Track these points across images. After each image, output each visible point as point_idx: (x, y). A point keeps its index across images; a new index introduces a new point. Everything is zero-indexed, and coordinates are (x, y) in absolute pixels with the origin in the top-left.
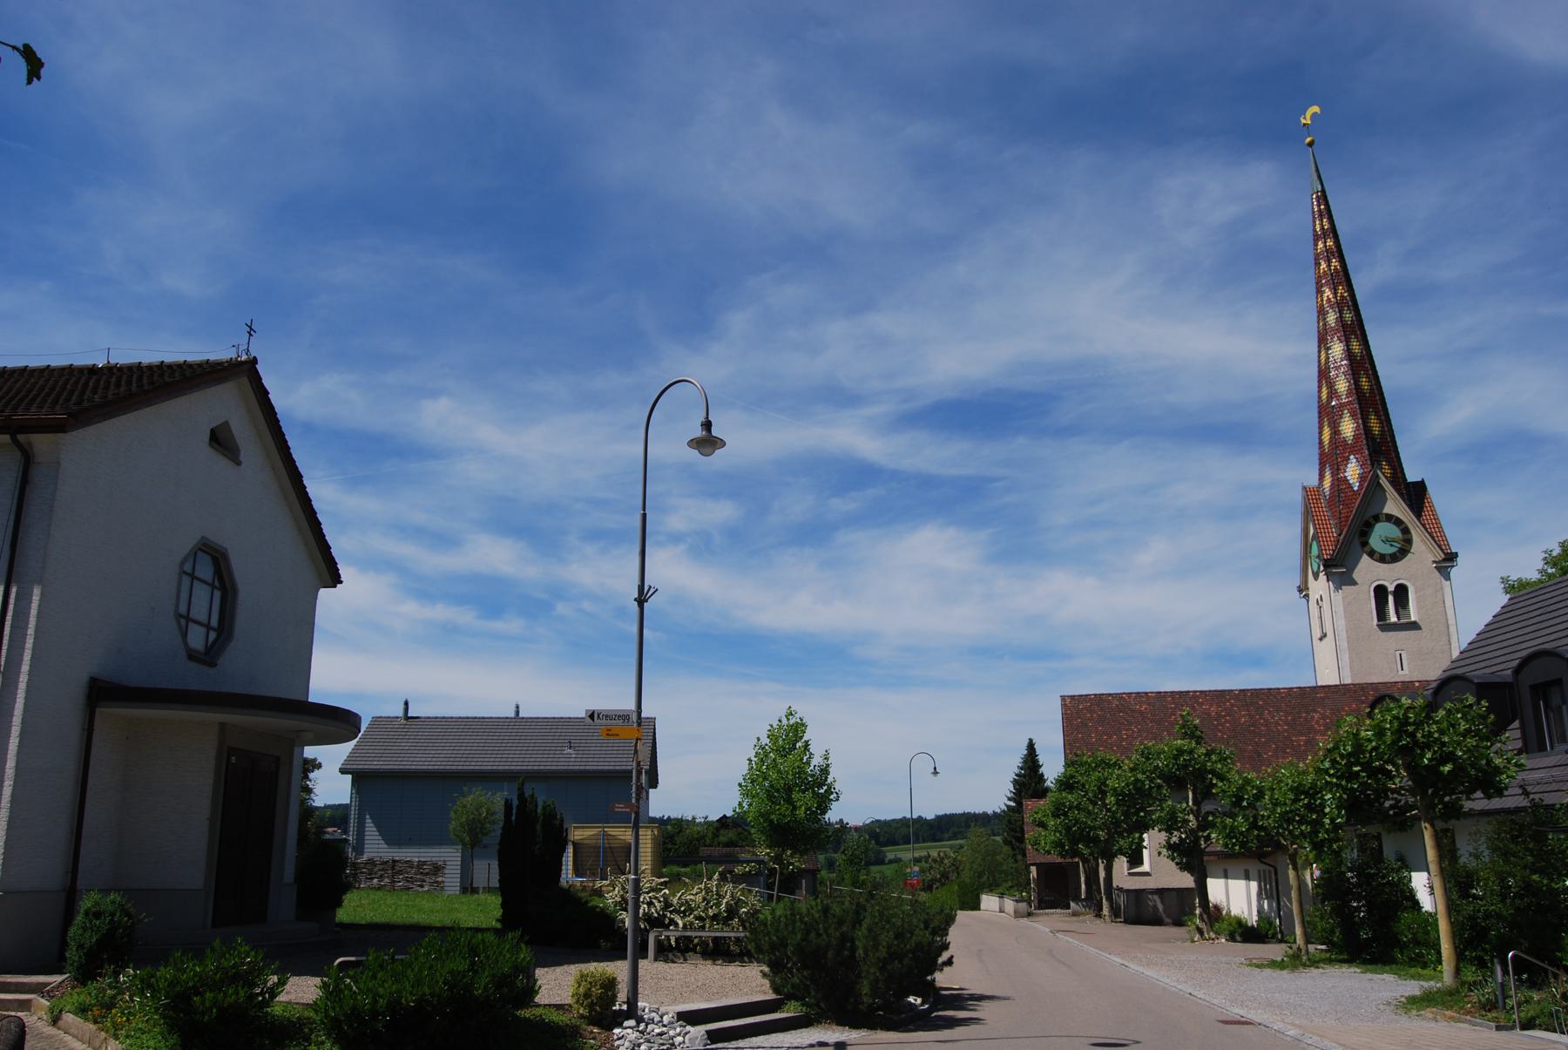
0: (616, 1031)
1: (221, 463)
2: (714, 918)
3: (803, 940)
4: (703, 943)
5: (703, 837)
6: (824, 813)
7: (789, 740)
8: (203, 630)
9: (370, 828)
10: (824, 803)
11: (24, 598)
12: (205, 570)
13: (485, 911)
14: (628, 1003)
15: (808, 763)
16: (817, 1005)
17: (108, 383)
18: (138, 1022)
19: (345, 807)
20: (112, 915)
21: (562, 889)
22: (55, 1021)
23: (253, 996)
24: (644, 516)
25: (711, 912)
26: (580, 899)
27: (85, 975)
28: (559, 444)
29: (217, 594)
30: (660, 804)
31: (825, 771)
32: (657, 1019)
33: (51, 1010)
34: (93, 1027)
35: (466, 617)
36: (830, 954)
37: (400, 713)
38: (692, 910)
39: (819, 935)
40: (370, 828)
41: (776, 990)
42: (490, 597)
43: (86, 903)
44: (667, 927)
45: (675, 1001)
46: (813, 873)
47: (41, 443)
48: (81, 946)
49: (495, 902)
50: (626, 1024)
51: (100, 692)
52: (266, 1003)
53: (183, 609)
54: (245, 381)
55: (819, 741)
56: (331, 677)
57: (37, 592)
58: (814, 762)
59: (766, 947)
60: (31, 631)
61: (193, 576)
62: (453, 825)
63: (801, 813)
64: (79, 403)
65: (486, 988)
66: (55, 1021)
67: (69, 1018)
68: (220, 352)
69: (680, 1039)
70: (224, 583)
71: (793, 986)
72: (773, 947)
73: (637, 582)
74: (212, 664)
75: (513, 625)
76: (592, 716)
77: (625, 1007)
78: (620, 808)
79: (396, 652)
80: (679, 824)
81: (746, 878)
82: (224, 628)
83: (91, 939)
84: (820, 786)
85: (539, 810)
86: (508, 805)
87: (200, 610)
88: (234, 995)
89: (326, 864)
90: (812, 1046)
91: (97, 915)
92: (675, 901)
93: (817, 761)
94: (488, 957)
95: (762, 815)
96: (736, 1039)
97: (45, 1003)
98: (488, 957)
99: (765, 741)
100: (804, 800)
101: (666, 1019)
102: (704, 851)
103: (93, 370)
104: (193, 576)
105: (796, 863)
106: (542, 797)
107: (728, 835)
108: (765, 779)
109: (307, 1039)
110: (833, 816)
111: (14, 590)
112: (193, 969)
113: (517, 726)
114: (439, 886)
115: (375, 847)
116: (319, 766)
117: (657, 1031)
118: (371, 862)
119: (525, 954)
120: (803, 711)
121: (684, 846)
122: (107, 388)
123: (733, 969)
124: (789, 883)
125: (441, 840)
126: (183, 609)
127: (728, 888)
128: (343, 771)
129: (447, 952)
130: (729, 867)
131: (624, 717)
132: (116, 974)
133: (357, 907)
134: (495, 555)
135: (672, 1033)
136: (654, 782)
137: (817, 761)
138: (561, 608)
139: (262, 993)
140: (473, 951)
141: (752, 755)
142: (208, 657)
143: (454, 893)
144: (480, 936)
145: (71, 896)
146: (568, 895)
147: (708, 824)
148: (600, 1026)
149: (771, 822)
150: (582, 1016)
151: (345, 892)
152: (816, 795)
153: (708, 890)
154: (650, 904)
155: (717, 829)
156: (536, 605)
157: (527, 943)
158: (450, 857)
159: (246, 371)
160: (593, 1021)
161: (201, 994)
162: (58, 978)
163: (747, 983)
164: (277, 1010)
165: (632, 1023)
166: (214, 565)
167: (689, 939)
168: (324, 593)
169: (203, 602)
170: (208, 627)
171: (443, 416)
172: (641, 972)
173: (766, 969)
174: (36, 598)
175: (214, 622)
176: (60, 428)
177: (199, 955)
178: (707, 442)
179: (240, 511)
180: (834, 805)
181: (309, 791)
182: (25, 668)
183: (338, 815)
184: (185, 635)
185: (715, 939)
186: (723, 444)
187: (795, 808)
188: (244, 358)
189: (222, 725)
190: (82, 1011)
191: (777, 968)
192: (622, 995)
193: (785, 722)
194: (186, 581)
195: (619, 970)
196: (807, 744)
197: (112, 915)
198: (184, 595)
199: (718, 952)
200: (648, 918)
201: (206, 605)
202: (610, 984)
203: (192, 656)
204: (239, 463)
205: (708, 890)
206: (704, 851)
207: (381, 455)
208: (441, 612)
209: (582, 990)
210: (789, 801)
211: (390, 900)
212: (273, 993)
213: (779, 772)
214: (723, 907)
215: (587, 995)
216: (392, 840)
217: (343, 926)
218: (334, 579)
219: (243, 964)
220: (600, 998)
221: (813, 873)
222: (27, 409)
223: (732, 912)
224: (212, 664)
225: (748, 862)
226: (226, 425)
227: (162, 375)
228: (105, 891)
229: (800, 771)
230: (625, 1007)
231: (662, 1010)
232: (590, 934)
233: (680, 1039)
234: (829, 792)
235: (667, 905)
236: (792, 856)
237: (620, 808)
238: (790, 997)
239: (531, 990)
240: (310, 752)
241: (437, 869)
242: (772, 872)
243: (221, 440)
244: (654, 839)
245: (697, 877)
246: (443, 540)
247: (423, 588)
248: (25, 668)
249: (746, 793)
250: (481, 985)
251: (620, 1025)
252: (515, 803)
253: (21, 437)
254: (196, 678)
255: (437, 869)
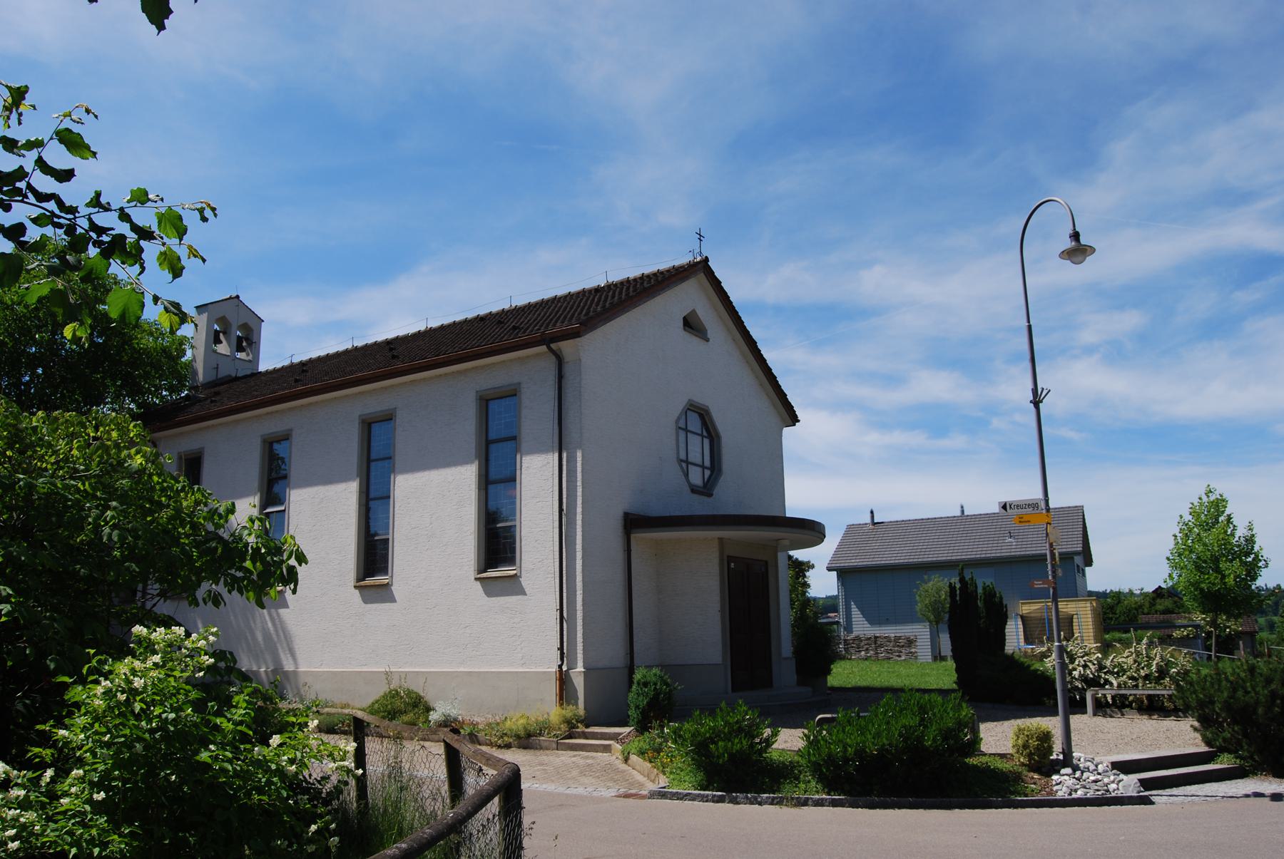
0: (1055, 777)
1: (693, 341)
2: (1147, 677)
3: (1230, 697)
4: (1138, 700)
5: (1141, 606)
6: (1254, 579)
7: (1212, 514)
8: (699, 470)
9: (855, 612)
10: (1252, 570)
11: (572, 460)
12: (694, 423)
13: (944, 676)
14: (1063, 753)
15: (1233, 535)
16: (1251, 757)
17: (607, 297)
18: (678, 762)
19: (836, 597)
20: (655, 684)
21: (1011, 658)
22: (626, 760)
23: (752, 746)
24: (1030, 327)
25: (1143, 673)
26: (1022, 664)
27: (643, 728)
28: (970, 287)
29: (706, 442)
30: (1098, 578)
31: (1250, 540)
32: (1092, 767)
33: (623, 752)
34: (649, 765)
35: (917, 439)
36: (1260, 711)
37: (868, 520)
38: (1125, 671)
39: (1247, 692)
40: (855, 612)
41: (1208, 743)
42: (935, 420)
43: (638, 676)
44: (1102, 686)
45: (1109, 752)
46: (1252, 635)
47: (566, 347)
48: (637, 707)
49: (951, 664)
50: (1063, 771)
51: (633, 523)
52: (765, 750)
53: (683, 456)
54: (702, 276)
55: (1242, 516)
56: (799, 499)
57: (579, 454)
58: (1238, 533)
59: (1194, 704)
60: (579, 483)
61: (686, 430)
62: (919, 607)
63: (1230, 581)
64: (587, 314)
65: (934, 740)
66: (626, 760)
67: (634, 758)
68: (683, 260)
69: (1113, 786)
70: (710, 432)
71: (1224, 740)
72: (1202, 705)
73: (1030, 386)
74: (710, 495)
75: (957, 441)
76: (1004, 507)
77: (1061, 757)
78: (1038, 584)
79: (853, 476)
80: (1118, 596)
81: (1183, 642)
82: (715, 466)
83: (644, 702)
84: (1247, 554)
85: (980, 591)
86: (952, 587)
87: (695, 456)
88: (739, 744)
89: (818, 639)
90: (1247, 796)
91: (646, 684)
92: (1108, 663)
93: (1241, 532)
94: (934, 714)
95: (1192, 584)
96: (1171, 787)
97: (619, 747)
98: (934, 714)
99: (1187, 517)
100: (1232, 570)
101: (1100, 768)
102: (1142, 619)
103: (598, 290)
104: (686, 430)
105: (1233, 626)
106: (983, 580)
107: (1162, 604)
108: (1191, 552)
109: (797, 778)
110: (1260, 582)
111: (565, 455)
112: (709, 724)
113: (963, 522)
114: (913, 655)
115: (862, 627)
116: (813, 567)
117: (1092, 778)
118: (858, 638)
119: (967, 711)
120: (1222, 487)
121: (1119, 615)
122: (605, 301)
123: (1169, 723)
124: (1227, 645)
125: (911, 619)
126: (683, 456)
127: (1157, 651)
128: (829, 569)
129: (901, 710)
130: (1167, 631)
131: (1033, 505)
132: (662, 727)
133: (842, 674)
134: (936, 386)
135: (1106, 780)
136: (1089, 562)
137: (1241, 532)
138: (996, 423)
139: (760, 743)
140: (922, 709)
141: (1177, 532)
142: (706, 490)
143: (921, 661)
144: (926, 697)
145: (631, 670)
146: (1012, 662)
147: (1145, 595)
148: (1040, 773)
149: (1202, 590)
150: (1023, 764)
151: (832, 662)
152: (1244, 564)
153: (1138, 654)
154: (1085, 666)
155: (1154, 599)
156: (974, 423)
157: (968, 701)
158: (921, 632)
159: (701, 268)
160: (1032, 768)
161: (716, 743)
162: (626, 730)
163: (1180, 736)
164: (775, 756)
165: (1068, 770)
166: (700, 419)
167: (1125, 697)
168: (787, 431)
169: (697, 449)
170: (703, 467)
171: (886, 279)
172: (1073, 726)
173: (1196, 724)
174: (579, 459)
175: (707, 463)
176: (576, 334)
177: (712, 713)
178: (1078, 251)
179: (713, 375)
180: (1264, 572)
181: (806, 585)
182: (579, 510)
183: (830, 605)
184: (687, 475)
185: (1149, 696)
186: (1093, 250)
187: (1224, 577)
188: (699, 259)
189: (721, 540)
190: (642, 753)
191: (1207, 723)
192: (1058, 746)
193: (1205, 499)
194: (682, 434)
195: (1052, 724)
196: (1229, 517)
197: (655, 684)
198: (682, 445)
199: (1152, 707)
200: (1084, 678)
201: (699, 450)
202: (1046, 737)
203: (694, 490)
204: (707, 340)
205: (1138, 654)
206: (1142, 619)
207: (828, 320)
208: (898, 438)
209: (1020, 742)
210: (1217, 570)
211: (874, 668)
212: (768, 742)
213: (1205, 545)
214: (1154, 668)
215: (1025, 746)
216: (873, 620)
217: (833, 689)
218: (794, 419)
219: (744, 720)
220: (1037, 748)
221: (1252, 635)
222: (554, 325)
223: (1162, 672)
224: (710, 495)
225: (1185, 627)
226: (693, 312)
227: (649, 282)
228: (649, 667)
229: (1225, 542)
230: (1061, 757)
231: (1097, 759)
232: (1025, 691)
233: (1113, 786)
234: (1257, 559)
235: (1101, 667)
236: (1228, 620)
237: (1038, 584)
238: (1222, 750)
239: (973, 746)
240: (800, 554)
241: (910, 642)
242: (1209, 634)
243: (691, 324)
244: (1094, 610)
245: (1127, 644)
246: (892, 380)
247: (881, 420)
248: (579, 510)
249: (1175, 566)
250: (930, 739)
251: (1058, 772)
252: (958, 586)
253: (553, 346)
254: (700, 506)
255: (910, 642)
